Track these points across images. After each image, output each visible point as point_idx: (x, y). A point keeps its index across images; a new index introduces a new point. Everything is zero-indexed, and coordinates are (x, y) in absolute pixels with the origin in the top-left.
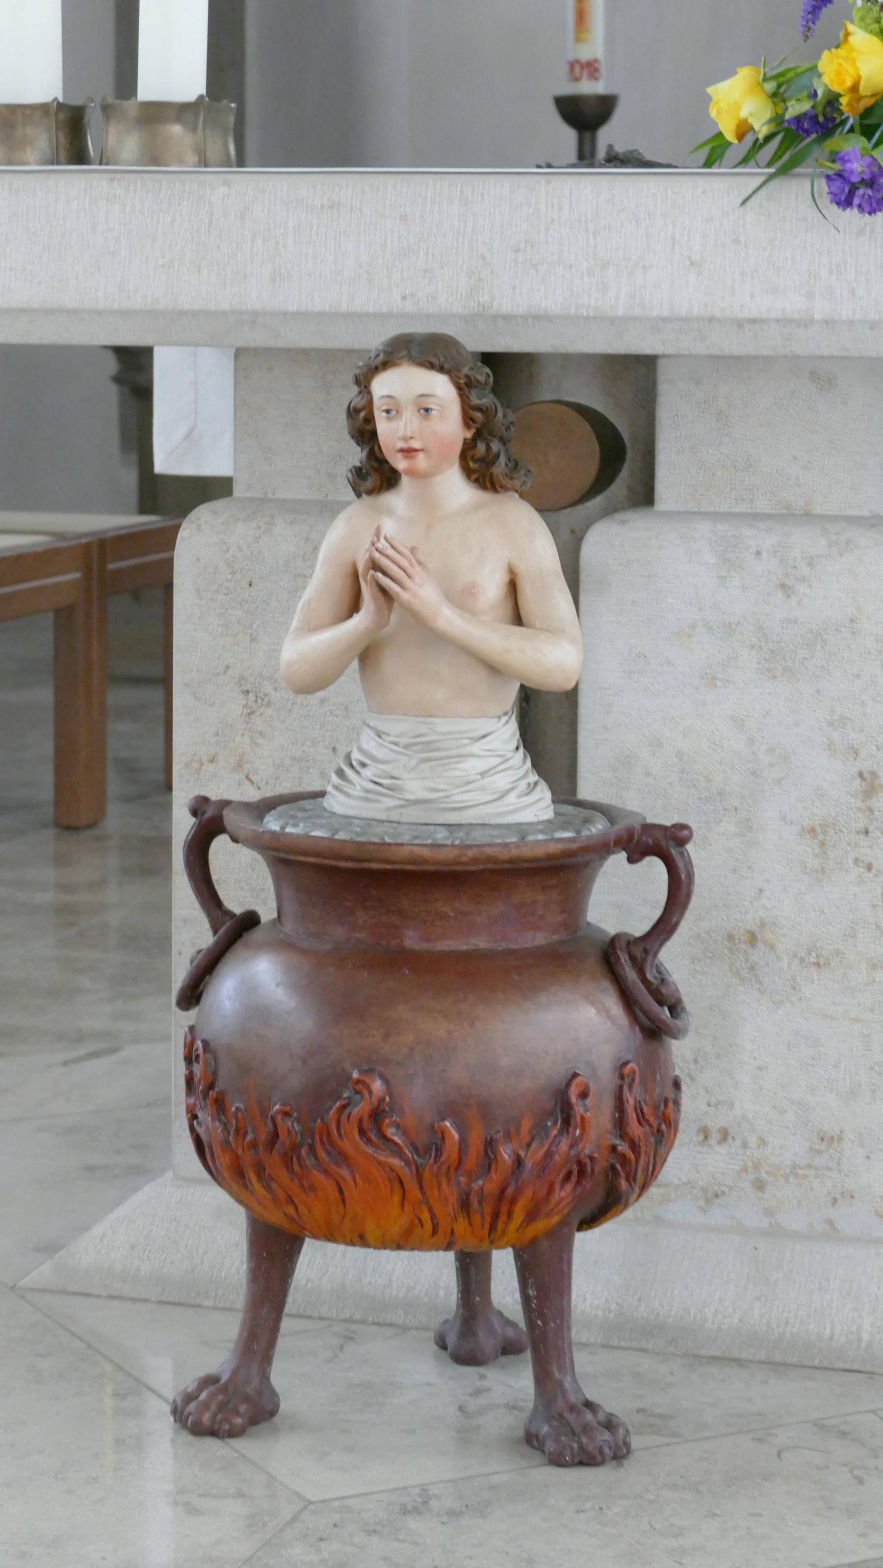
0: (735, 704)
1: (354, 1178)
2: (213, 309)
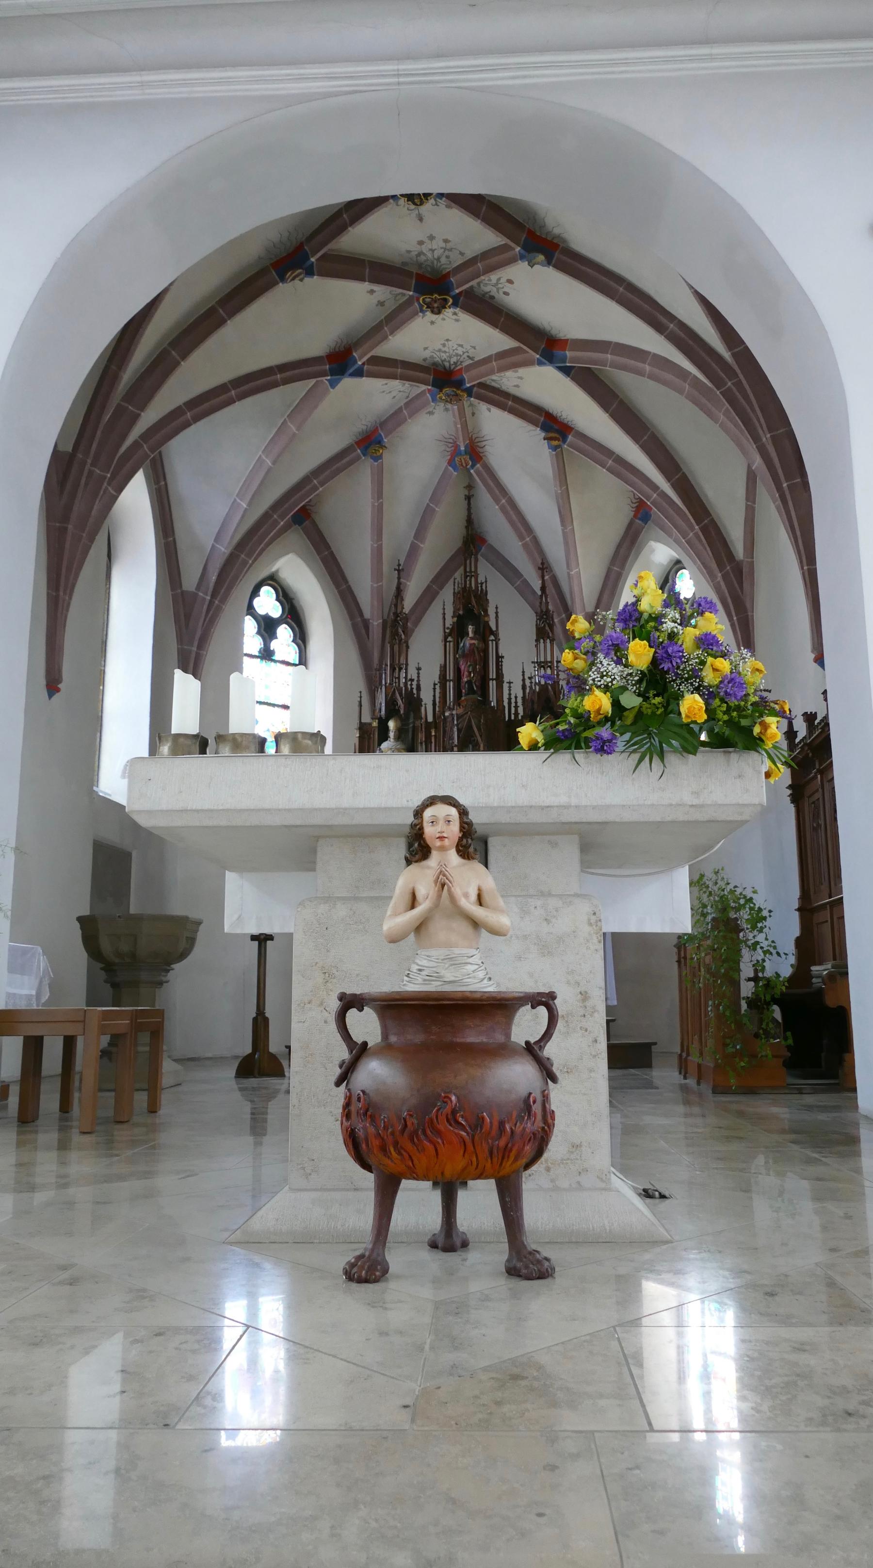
1: (443, 1143)
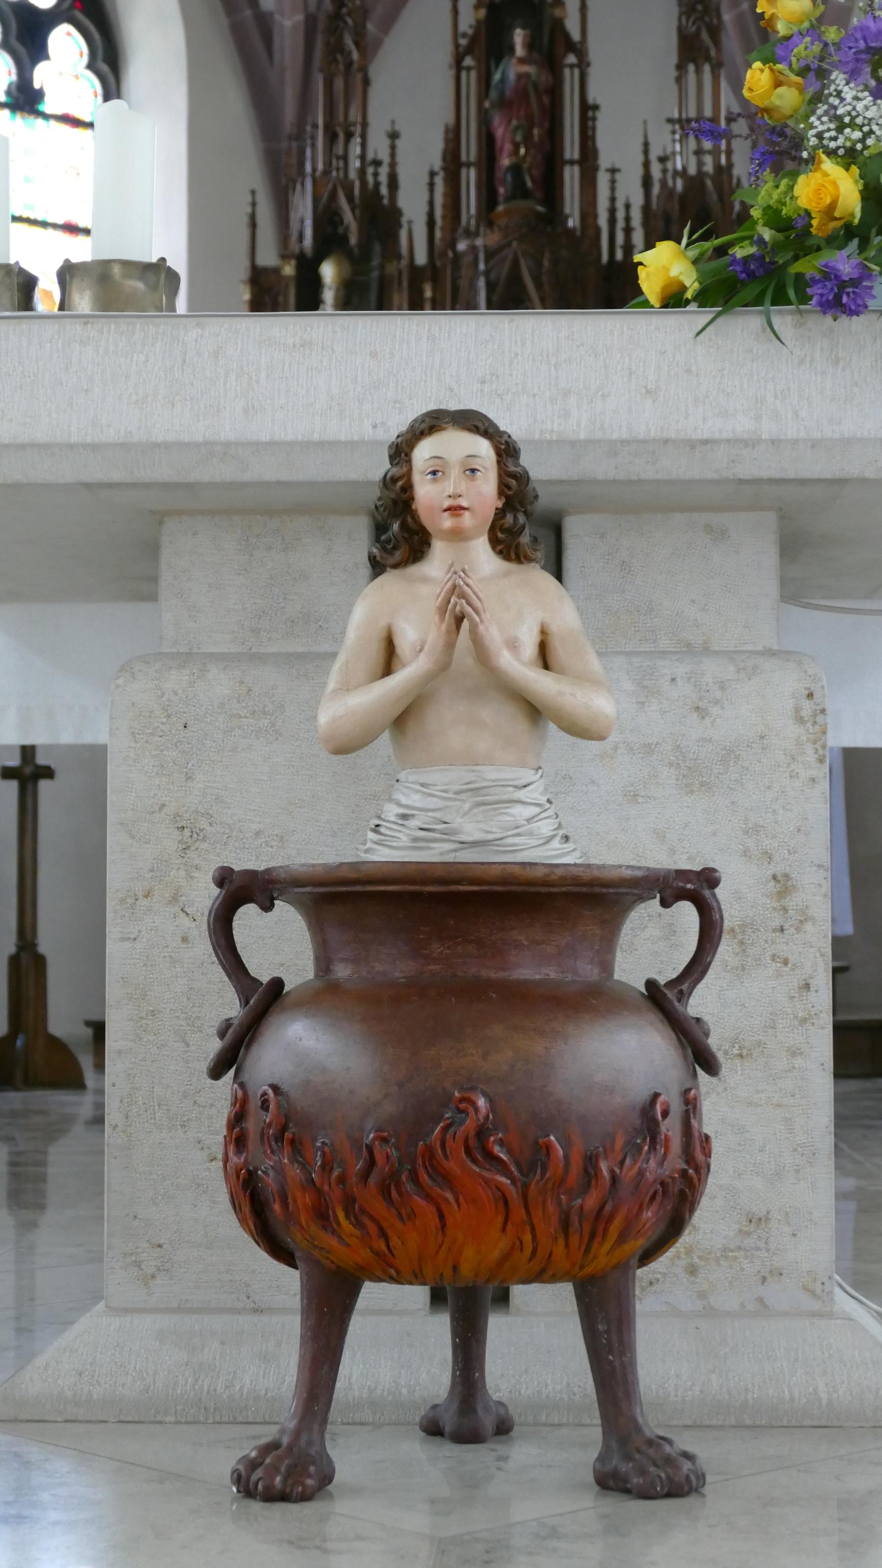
0: (657, 818)
1: (457, 1201)
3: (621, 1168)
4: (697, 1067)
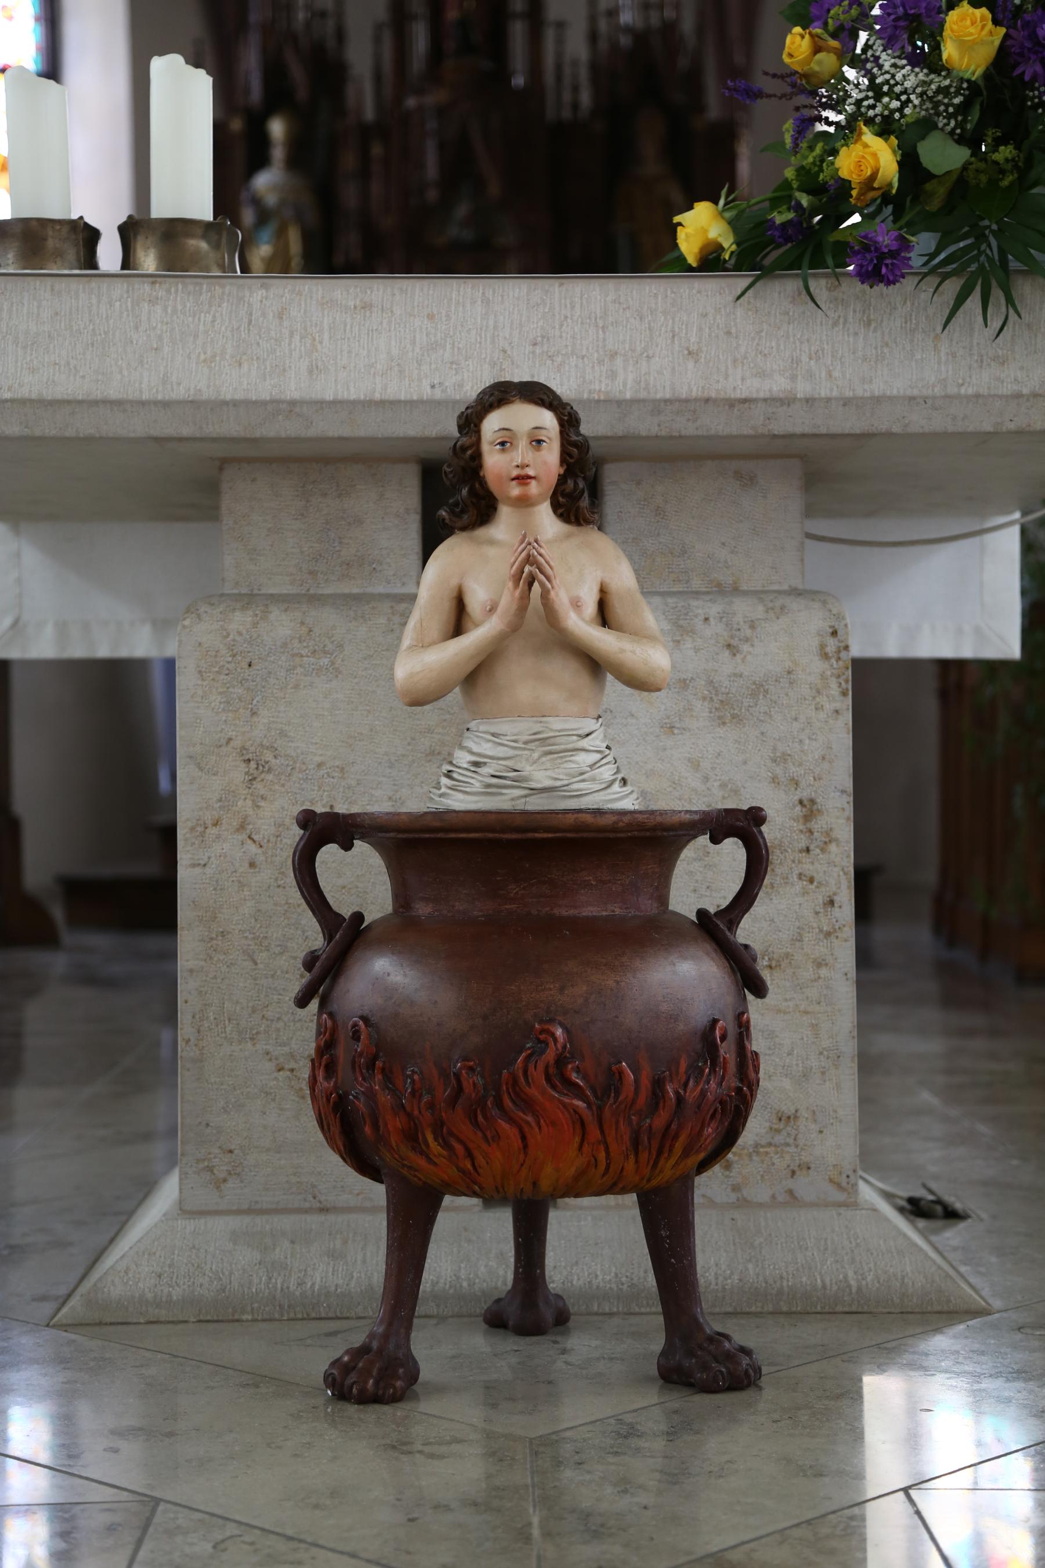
2: (254, 399)
3: (685, 1091)
4: (746, 990)
